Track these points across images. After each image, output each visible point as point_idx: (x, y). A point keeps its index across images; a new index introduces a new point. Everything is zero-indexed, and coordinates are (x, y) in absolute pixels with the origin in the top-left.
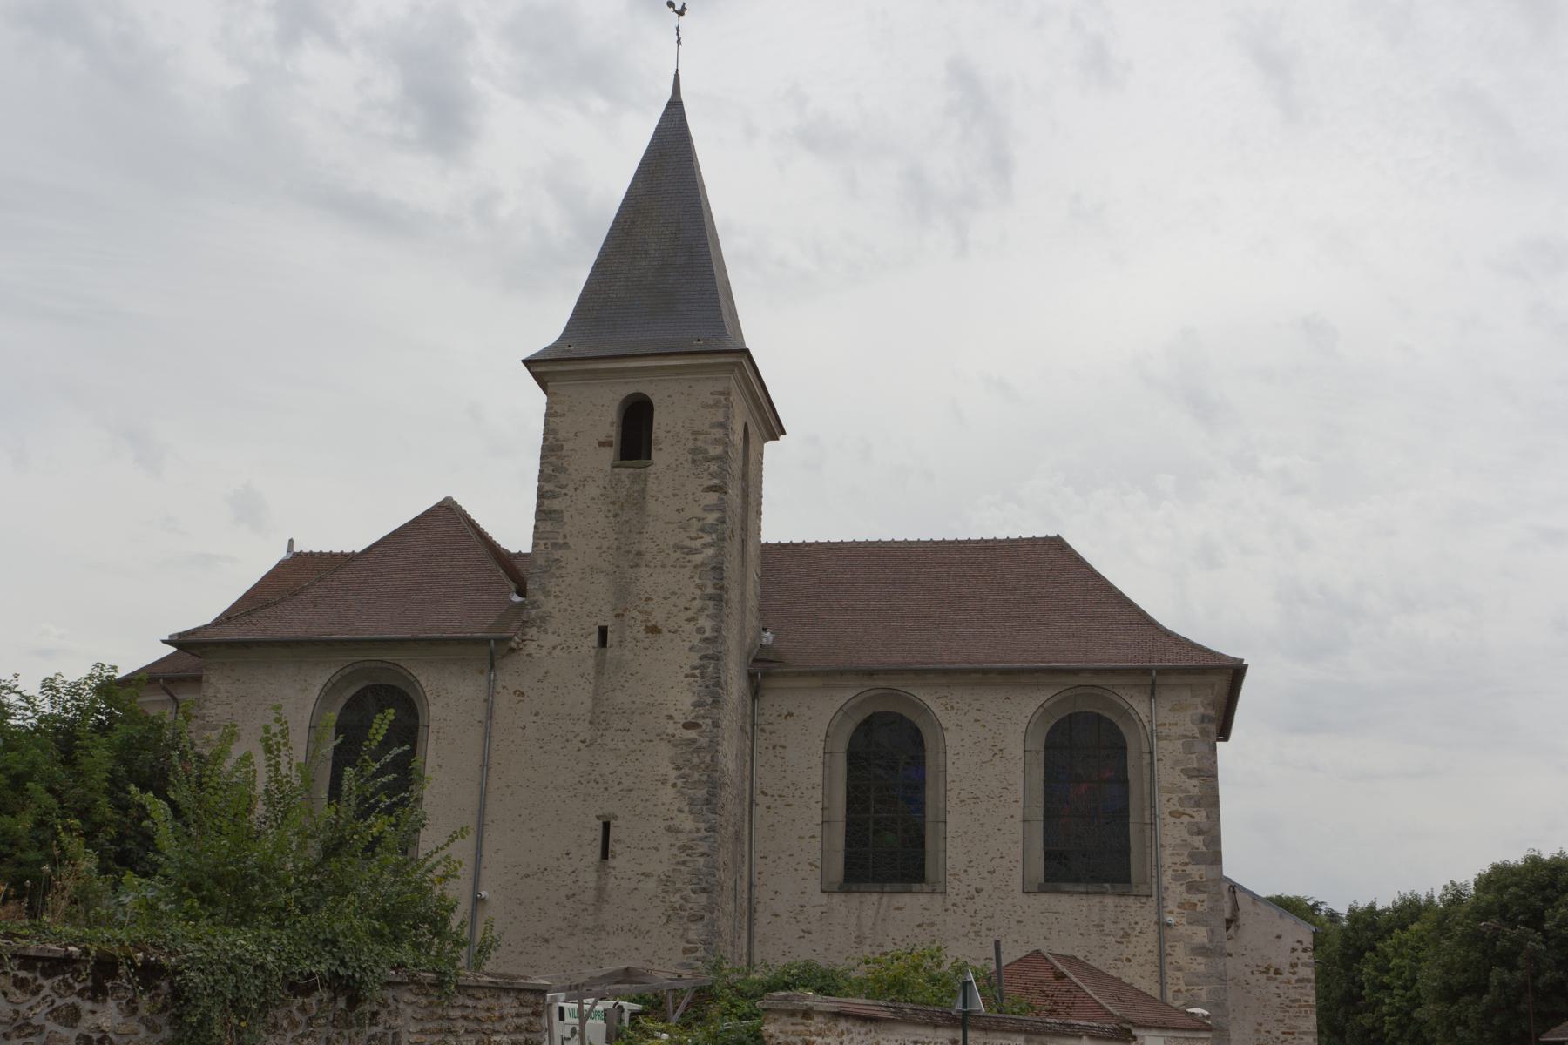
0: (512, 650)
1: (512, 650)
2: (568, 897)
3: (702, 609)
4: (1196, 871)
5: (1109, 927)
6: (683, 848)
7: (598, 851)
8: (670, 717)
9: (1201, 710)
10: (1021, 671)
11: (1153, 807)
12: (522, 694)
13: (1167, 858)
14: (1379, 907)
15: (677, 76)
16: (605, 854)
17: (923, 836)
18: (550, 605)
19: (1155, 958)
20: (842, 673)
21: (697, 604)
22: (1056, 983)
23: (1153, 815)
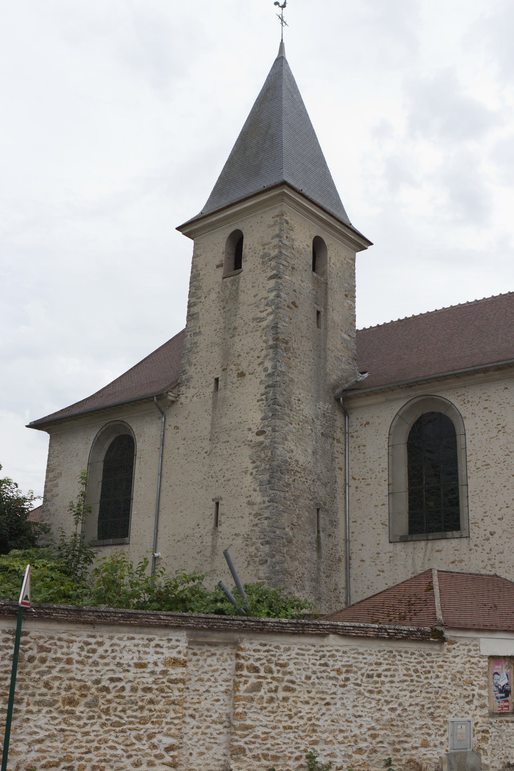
0: (173, 402)
2: (198, 553)
3: (267, 356)
6: (257, 515)
7: (213, 521)
8: (250, 429)
12: (178, 428)
15: (282, 40)
16: (217, 523)
21: (264, 353)
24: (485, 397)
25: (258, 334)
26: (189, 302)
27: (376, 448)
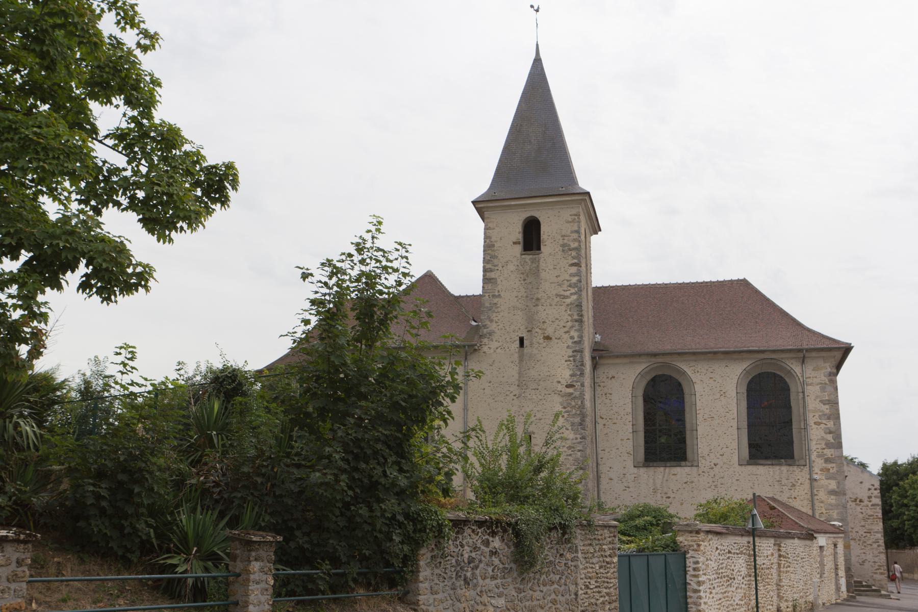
1: (475, 350)
3: (572, 327)
4: (829, 452)
5: (784, 481)
6: (569, 448)
8: (559, 382)
9: (829, 370)
10: (734, 352)
11: (805, 420)
13: (813, 446)
14: (899, 463)
15: (537, 45)
17: (685, 438)
18: (493, 327)
19: (809, 496)
20: (640, 355)
21: (569, 324)
22: (771, 512)
23: (806, 424)
24: (710, 370)
25: (563, 308)
26: (484, 267)
27: (621, 399)
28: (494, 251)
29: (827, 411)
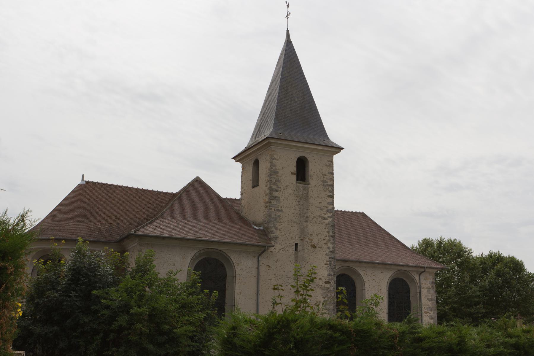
3: (329, 240)
9: (432, 280)
15: (288, 31)
21: (327, 238)
28: (277, 176)
29: (431, 305)
